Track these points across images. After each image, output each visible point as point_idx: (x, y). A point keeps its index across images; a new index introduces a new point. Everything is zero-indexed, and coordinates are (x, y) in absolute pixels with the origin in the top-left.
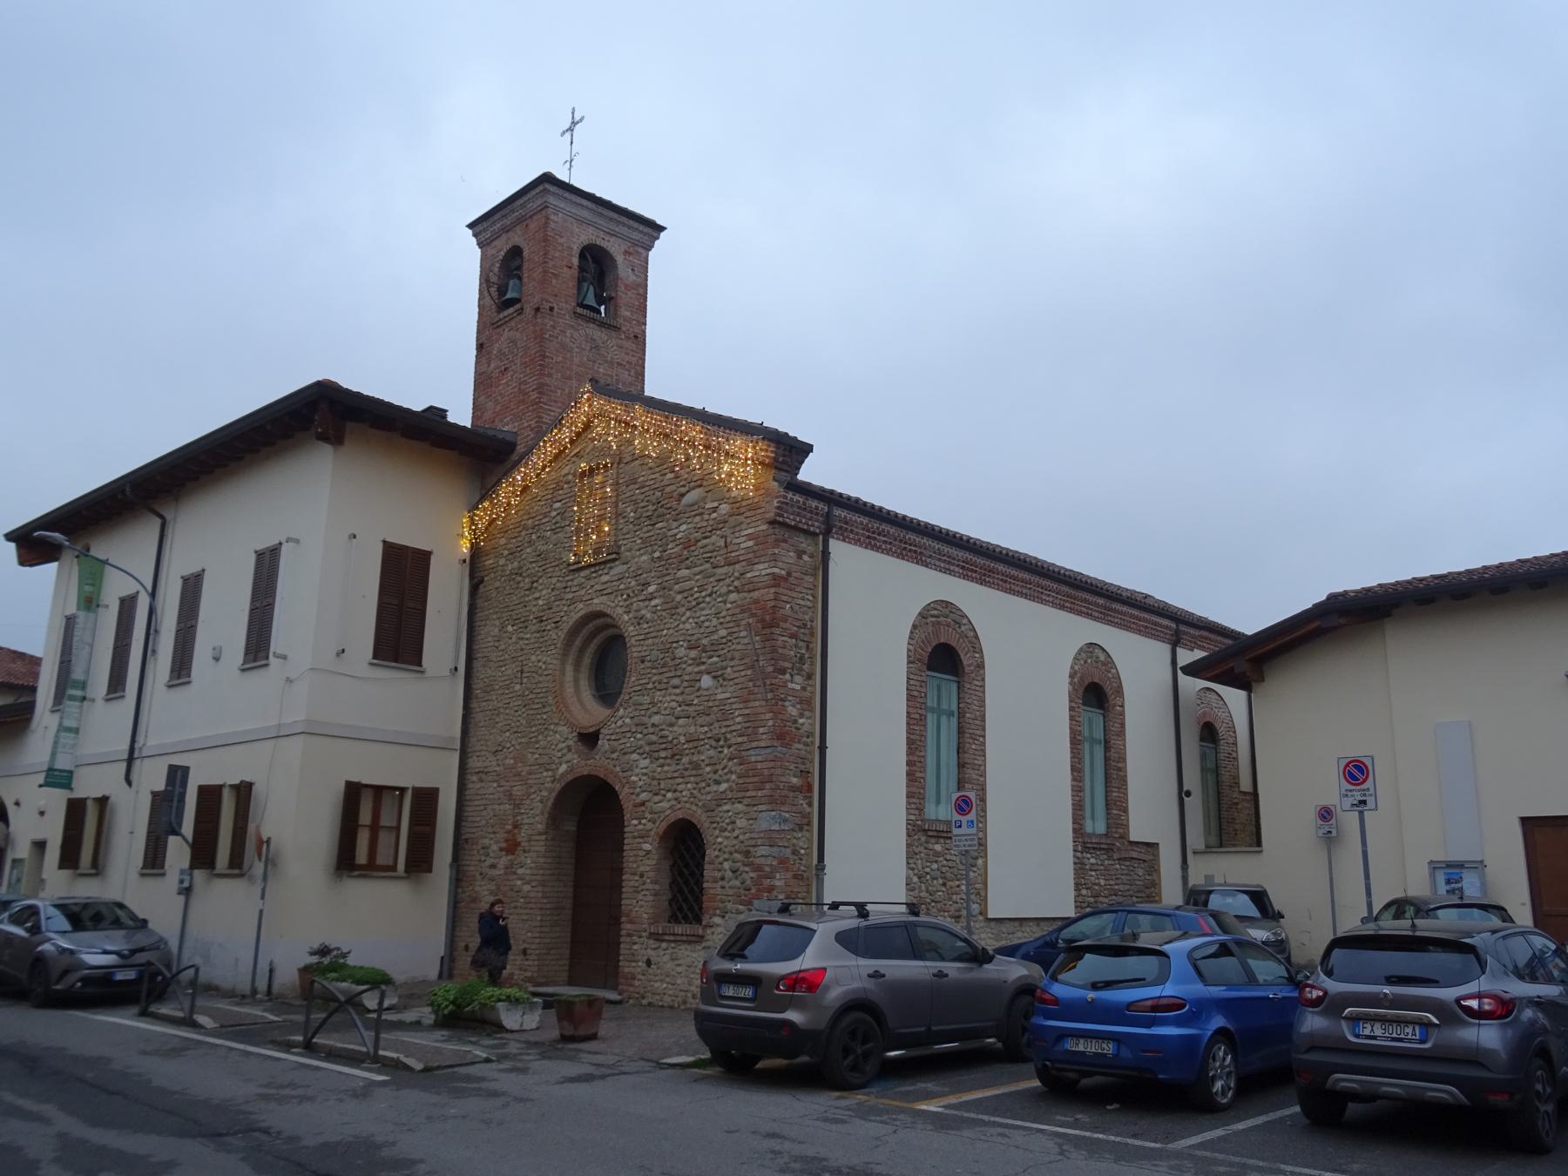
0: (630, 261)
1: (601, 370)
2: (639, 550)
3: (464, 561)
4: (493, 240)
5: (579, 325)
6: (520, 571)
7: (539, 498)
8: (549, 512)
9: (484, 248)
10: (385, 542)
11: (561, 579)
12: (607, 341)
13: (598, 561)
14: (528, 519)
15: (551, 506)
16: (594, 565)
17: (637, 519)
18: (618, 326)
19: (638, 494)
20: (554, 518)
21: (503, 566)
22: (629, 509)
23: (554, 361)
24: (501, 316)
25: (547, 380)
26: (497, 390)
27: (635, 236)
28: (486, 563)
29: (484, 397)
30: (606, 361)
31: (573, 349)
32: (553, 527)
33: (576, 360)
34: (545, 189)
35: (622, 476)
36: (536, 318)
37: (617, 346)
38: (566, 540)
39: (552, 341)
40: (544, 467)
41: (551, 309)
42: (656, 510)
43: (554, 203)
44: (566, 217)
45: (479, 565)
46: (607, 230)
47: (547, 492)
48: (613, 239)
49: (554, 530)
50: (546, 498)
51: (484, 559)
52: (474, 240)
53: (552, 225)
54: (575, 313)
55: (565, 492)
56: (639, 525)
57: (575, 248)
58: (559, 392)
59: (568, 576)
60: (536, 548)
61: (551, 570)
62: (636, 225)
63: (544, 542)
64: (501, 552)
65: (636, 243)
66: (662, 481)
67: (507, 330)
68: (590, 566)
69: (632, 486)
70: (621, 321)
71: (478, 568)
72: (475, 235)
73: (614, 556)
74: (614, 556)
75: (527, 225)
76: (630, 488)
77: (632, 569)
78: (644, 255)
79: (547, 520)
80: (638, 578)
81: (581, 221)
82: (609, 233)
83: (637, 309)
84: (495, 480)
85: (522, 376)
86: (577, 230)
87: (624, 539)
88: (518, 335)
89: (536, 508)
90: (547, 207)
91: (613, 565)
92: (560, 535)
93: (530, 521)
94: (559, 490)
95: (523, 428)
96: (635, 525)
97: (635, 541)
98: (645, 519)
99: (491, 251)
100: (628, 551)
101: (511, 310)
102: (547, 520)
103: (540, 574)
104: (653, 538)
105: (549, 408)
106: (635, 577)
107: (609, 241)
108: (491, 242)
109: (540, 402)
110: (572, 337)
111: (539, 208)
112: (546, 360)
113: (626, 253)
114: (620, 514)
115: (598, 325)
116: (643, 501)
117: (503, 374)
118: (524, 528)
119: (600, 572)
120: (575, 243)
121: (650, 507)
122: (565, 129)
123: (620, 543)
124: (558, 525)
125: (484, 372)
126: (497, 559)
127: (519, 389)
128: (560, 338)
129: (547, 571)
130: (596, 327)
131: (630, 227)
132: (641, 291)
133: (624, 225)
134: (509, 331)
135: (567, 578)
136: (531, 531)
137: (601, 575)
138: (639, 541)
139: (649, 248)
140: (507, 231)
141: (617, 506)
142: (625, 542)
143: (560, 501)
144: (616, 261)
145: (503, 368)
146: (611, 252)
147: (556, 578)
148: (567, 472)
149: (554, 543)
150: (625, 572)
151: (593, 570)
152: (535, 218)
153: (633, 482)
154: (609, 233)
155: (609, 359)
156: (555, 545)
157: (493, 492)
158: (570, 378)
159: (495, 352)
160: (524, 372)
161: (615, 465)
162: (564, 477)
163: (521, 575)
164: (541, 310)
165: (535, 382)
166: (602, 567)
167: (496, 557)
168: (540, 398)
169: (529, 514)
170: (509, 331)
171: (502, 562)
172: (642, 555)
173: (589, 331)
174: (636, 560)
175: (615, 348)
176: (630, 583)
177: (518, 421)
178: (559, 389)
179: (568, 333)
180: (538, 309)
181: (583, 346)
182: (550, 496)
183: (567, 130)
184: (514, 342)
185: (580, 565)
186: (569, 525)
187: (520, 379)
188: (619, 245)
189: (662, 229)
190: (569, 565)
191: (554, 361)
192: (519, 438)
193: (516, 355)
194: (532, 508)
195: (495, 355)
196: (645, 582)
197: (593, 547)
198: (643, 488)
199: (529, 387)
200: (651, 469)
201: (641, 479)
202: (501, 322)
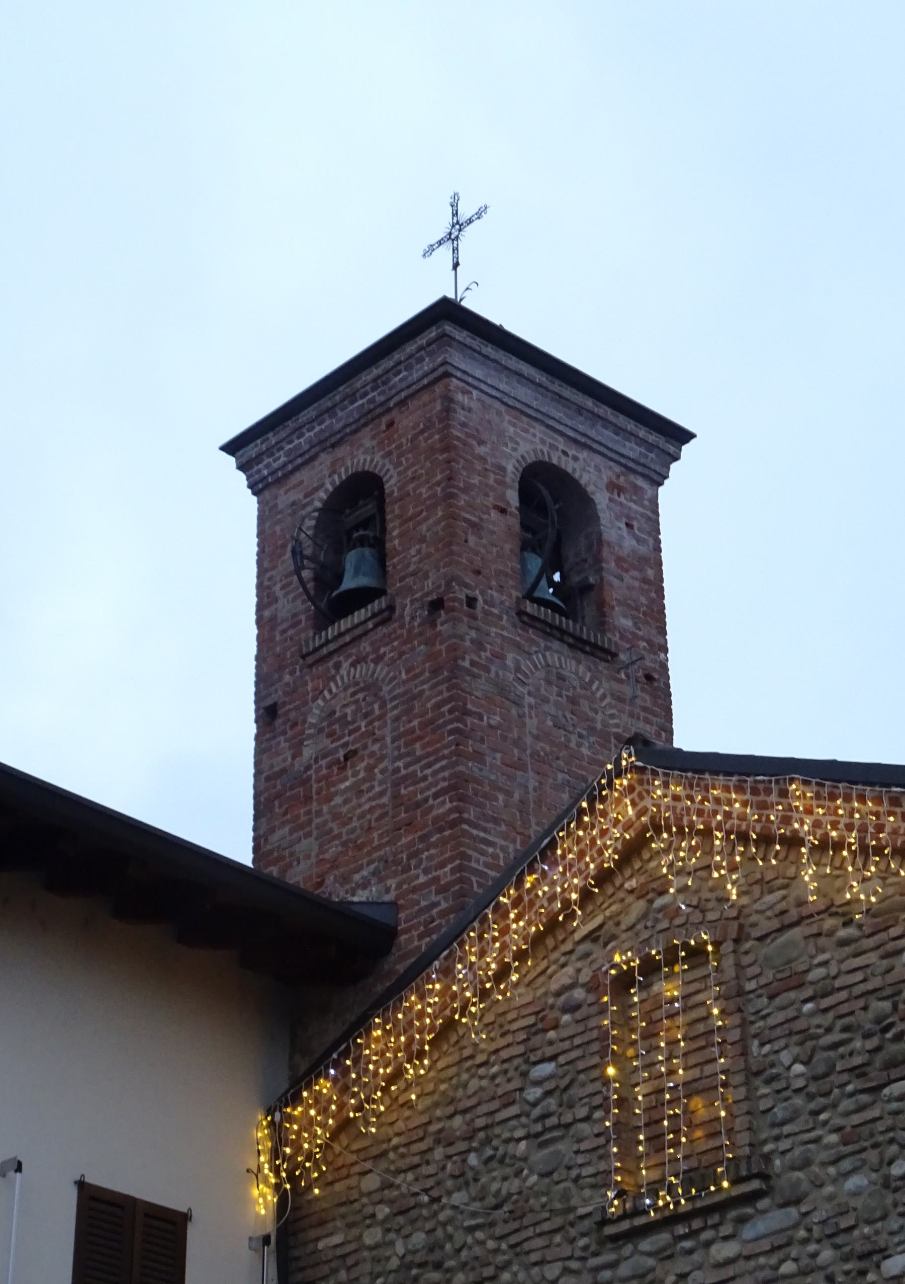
0: (621, 504)
1: (585, 751)
2: (835, 1162)
3: (266, 1240)
4: (292, 472)
5: (533, 642)
6: (437, 1256)
7: (480, 1058)
8: (521, 1090)
9: (267, 494)
10: (81, 1185)
11: (574, 1265)
12: (591, 682)
13: (699, 1204)
14: (451, 1116)
15: (524, 1074)
16: (685, 1217)
17: (816, 1078)
18: (613, 649)
19: (812, 1014)
20: (534, 1105)
21: (376, 1247)
22: (785, 1057)
23: (485, 723)
24: (331, 632)
25: (470, 767)
26: (325, 808)
27: (631, 450)
28: (321, 1245)
29: (286, 829)
30: (592, 730)
31: (522, 698)
32: (539, 1127)
33: (532, 724)
34: (444, 335)
35: (751, 972)
36: (434, 625)
37: (612, 695)
38: (580, 1159)
39: (479, 676)
40: (503, 973)
41: (471, 602)
42: (878, 1049)
43: (463, 366)
44: (488, 400)
45: (296, 1253)
46: (572, 434)
47: (509, 1039)
48: (584, 455)
49: (537, 1135)
50: (504, 1054)
51: (312, 1234)
52: (242, 477)
53: (461, 415)
54: (521, 613)
55: (564, 1033)
56: (827, 1094)
57: (510, 468)
58: (501, 797)
59: (596, 1254)
60: (484, 1188)
61: (539, 1242)
62: (631, 425)
63: (508, 1171)
64: (369, 1210)
65: (631, 464)
66: (889, 970)
67: (346, 665)
68: (670, 1220)
69: (792, 995)
70: (617, 638)
71: (298, 1258)
72: (241, 467)
73: (755, 1185)
74: (755, 1185)
75: (391, 424)
76: (778, 1001)
77: (816, 1218)
78: (649, 493)
79: (514, 1110)
80: (839, 1240)
81: (519, 410)
82: (575, 441)
83: (645, 614)
84: (334, 1031)
85: (400, 764)
86: (512, 429)
87: (777, 1138)
88: (381, 671)
89: (474, 1084)
90: (447, 375)
91: (749, 1210)
92: (561, 1146)
93: (458, 1121)
94: (546, 1031)
95: (414, 890)
96: (811, 1097)
97: (817, 1140)
98: (845, 1077)
99: (285, 497)
100: (793, 1168)
101: (359, 616)
102: (514, 1110)
103: (500, 1259)
104: (880, 1126)
105: (482, 834)
106: (829, 1236)
107: (575, 459)
108: (286, 476)
109: (462, 821)
110: (518, 669)
111: (425, 381)
112: (469, 720)
113: (613, 487)
114: (758, 1074)
115: (571, 646)
116: (829, 1030)
117: (343, 768)
118: (438, 1141)
119: (706, 1235)
120: (508, 457)
121: (858, 1044)
122: (434, 240)
123: (768, 1148)
124: (553, 1120)
125: (284, 771)
126: (355, 1231)
127: (396, 796)
128: (493, 669)
129: (526, 1246)
130: (566, 649)
131: (618, 430)
132: (650, 573)
133: (606, 423)
134: (353, 665)
135: (593, 1262)
136: (461, 1146)
137: (708, 1244)
138: (834, 1138)
139: (659, 479)
140: (333, 446)
141: (745, 1053)
142: (784, 1145)
143: (553, 1058)
144: (592, 501)
145: (341, 754)
146: (583, 482)
147: (560, 1264)
148: (567, 981)
149: (542, 1168)
150: (796, 1226)
151: (681, 1230)
152: (412, 404)
153: (793, 982)
154: (575, 441)
155: (599, 726)
156: (549, 1174)
157: (346, 1054)
158: (520, 766)
159: (311, 720)
160: (408, 754)
161: (728, 947)
162: (558, 994)
163: (438, 1266)
164: (446, 604)
165: (446, 774)
166: (715, 1219)
167: (350, 1226)
168: (460, 811)
169: (452, 1101)
170: (353, 665)
171: (372, 1236)
172: (847, 1175)
173: (553, 658)
174: (829, 1189)
175: (608, 700)
176: (814, 1255)
177: (395, 874)
178: (500, 789)
179: (510, 658)
180: (437, 605)
181: (543, 692)
182: (521, 1049)
183: (470, 221)
184: (372, 688)
185: (639, 1221)
186: (587, 1119)
187: (397, 770)
188: (597, 468)
189: (685, 436)
190: (605, 1221)
191: (485, 723)
192: (402, 915)
193: (380, 717)
194: (465, 1086)
195: (312, 725)
196: (868, 1247)
197: (683, 1167)
198: (825, 995)
199: (428, 788)
200: (843, 943)
201: (820, 972)
202: (332, 647)
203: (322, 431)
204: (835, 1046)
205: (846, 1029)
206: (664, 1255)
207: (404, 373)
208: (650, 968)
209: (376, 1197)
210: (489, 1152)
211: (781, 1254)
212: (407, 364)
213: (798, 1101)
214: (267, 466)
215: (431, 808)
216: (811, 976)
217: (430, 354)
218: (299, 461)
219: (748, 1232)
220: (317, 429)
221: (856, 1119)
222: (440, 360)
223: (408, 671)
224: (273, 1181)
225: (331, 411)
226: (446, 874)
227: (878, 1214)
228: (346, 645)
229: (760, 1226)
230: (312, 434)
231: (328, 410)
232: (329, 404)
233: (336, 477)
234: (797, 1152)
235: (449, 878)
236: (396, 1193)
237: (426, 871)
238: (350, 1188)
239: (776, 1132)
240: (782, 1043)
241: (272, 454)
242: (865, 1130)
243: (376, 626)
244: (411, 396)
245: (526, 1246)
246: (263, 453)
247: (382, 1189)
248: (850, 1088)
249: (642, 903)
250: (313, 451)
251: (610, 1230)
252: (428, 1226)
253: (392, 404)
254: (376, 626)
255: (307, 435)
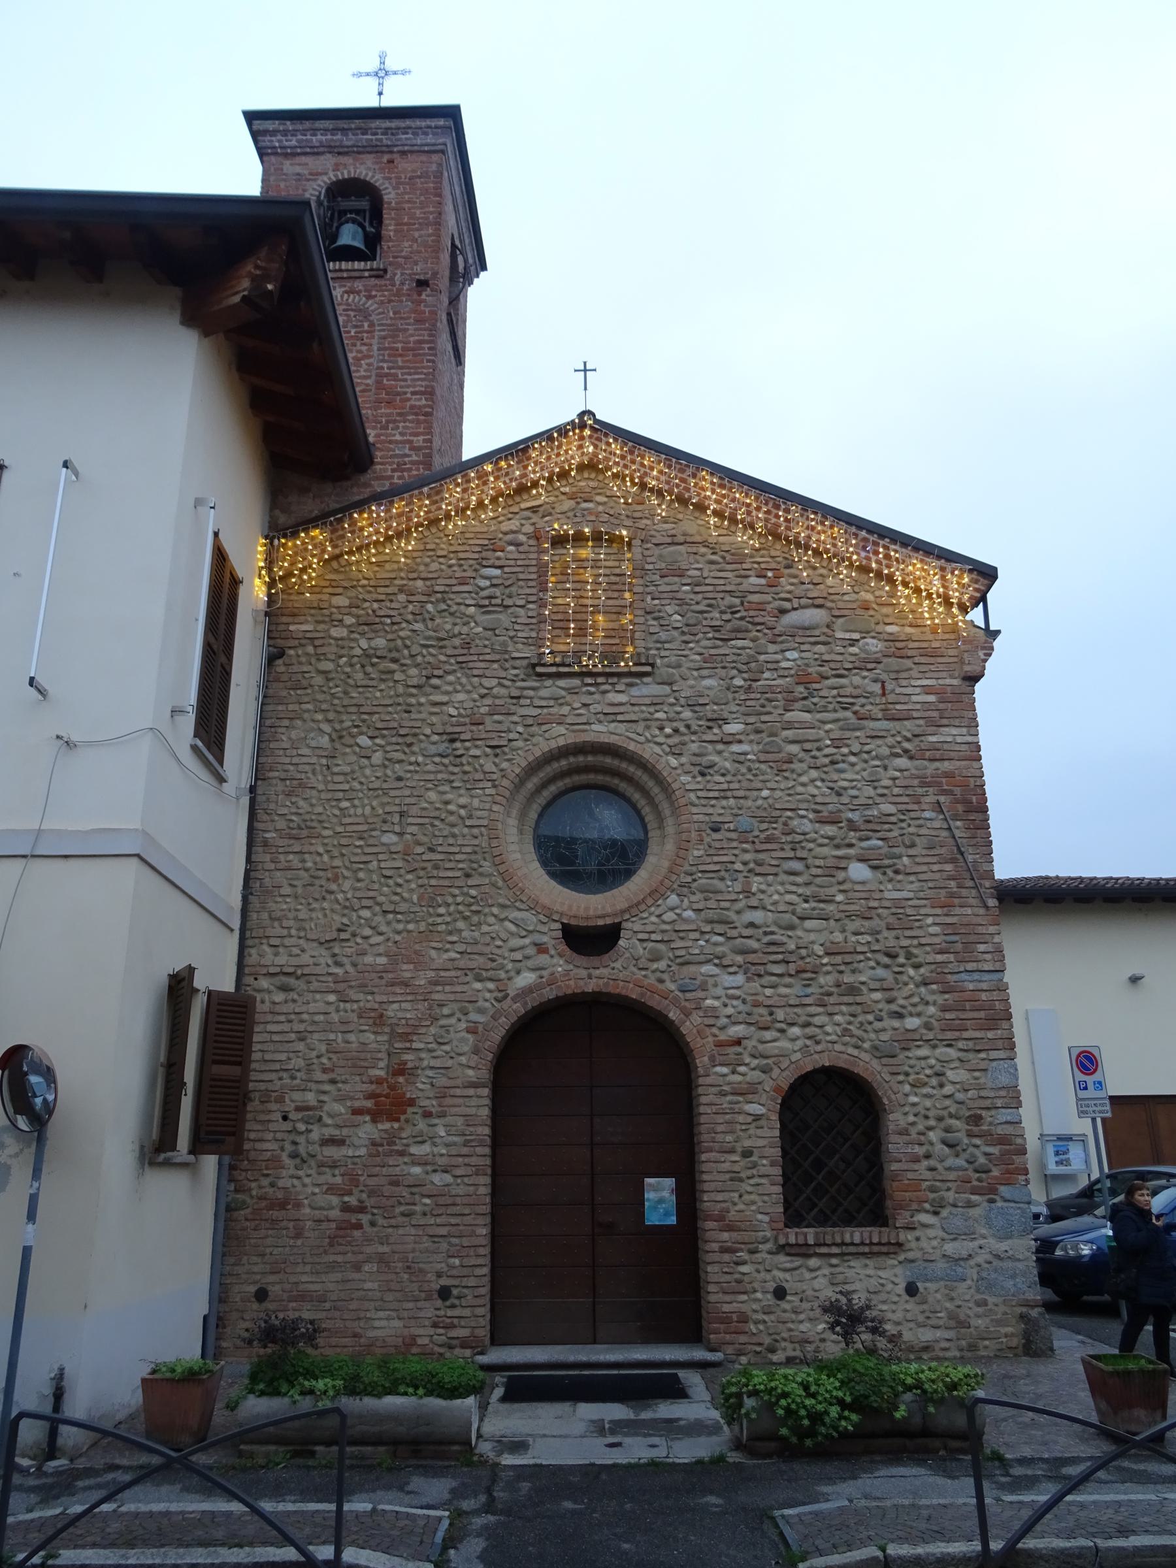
13: (608, 670)
20: (482, 589)
32: (486, 602)
42: (729, 621)
50: (461, 555)
69: (676, 579)
73: (648, 669)
74: (648, 669)
75: (391, 161)
76: (666, 580)
80: (697, 708)
85: (385, 365)
91: (638, 681)
95: (391, 442)
96: (683, 633)
98: (708, 629)
100: (669, 666)
116: (697, 603)
122: (399, 77)
137: (605, 692)
138: (698, 658)
140: (339, 153)
151: (589, 680)
153: (678, 572)
165: (423, 383)
187: (382, 368)
199: (408, 387)
203: (332, 140)
204: (702, 612)
205: (709, 606)
206: (571, 691)
207: (410, 136)
208: (579, 538)
209: (347, 611)
210: (444, 607)
211: (657, 708)
212: (416, 131)
213: (675, 633)
214: (279, 141)
215: (409, 399)
216: (690, 573)
217: (434, 134)
218: (308, 150)
219: (635, 691)
220: (329, 137)
221: (713, 651)
222: (441, 141)
223: (395, 313)
224: (267, 579)
225: (344, 131)
226: (419, 441)
227: (724, 701)
228: (343, 278)
229: (645, 691)
230: (324, 138)
231: (343, 130)
232: (346, 126)
233: (370, 174)
234: (673, 659)
235: (421, 444)
236: (362, 612)
237: (401, 434)
238: (321, 600)
239: (659, 645)
240: (668, 601)
241: (286, 135)
242: (719, 658)
243: (370, 276)
244: (412, 152)
245: (471, 665)
246: (279, 131)
247: (350, 607)
248: (710, 635)
249: (572, 502)
250: (321, 149)
251: (539, 669)
252: (390, 637)
253: (395, 149)
254: (370, 276)
255: (319, 137)
